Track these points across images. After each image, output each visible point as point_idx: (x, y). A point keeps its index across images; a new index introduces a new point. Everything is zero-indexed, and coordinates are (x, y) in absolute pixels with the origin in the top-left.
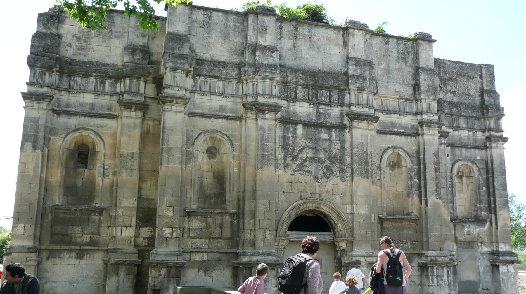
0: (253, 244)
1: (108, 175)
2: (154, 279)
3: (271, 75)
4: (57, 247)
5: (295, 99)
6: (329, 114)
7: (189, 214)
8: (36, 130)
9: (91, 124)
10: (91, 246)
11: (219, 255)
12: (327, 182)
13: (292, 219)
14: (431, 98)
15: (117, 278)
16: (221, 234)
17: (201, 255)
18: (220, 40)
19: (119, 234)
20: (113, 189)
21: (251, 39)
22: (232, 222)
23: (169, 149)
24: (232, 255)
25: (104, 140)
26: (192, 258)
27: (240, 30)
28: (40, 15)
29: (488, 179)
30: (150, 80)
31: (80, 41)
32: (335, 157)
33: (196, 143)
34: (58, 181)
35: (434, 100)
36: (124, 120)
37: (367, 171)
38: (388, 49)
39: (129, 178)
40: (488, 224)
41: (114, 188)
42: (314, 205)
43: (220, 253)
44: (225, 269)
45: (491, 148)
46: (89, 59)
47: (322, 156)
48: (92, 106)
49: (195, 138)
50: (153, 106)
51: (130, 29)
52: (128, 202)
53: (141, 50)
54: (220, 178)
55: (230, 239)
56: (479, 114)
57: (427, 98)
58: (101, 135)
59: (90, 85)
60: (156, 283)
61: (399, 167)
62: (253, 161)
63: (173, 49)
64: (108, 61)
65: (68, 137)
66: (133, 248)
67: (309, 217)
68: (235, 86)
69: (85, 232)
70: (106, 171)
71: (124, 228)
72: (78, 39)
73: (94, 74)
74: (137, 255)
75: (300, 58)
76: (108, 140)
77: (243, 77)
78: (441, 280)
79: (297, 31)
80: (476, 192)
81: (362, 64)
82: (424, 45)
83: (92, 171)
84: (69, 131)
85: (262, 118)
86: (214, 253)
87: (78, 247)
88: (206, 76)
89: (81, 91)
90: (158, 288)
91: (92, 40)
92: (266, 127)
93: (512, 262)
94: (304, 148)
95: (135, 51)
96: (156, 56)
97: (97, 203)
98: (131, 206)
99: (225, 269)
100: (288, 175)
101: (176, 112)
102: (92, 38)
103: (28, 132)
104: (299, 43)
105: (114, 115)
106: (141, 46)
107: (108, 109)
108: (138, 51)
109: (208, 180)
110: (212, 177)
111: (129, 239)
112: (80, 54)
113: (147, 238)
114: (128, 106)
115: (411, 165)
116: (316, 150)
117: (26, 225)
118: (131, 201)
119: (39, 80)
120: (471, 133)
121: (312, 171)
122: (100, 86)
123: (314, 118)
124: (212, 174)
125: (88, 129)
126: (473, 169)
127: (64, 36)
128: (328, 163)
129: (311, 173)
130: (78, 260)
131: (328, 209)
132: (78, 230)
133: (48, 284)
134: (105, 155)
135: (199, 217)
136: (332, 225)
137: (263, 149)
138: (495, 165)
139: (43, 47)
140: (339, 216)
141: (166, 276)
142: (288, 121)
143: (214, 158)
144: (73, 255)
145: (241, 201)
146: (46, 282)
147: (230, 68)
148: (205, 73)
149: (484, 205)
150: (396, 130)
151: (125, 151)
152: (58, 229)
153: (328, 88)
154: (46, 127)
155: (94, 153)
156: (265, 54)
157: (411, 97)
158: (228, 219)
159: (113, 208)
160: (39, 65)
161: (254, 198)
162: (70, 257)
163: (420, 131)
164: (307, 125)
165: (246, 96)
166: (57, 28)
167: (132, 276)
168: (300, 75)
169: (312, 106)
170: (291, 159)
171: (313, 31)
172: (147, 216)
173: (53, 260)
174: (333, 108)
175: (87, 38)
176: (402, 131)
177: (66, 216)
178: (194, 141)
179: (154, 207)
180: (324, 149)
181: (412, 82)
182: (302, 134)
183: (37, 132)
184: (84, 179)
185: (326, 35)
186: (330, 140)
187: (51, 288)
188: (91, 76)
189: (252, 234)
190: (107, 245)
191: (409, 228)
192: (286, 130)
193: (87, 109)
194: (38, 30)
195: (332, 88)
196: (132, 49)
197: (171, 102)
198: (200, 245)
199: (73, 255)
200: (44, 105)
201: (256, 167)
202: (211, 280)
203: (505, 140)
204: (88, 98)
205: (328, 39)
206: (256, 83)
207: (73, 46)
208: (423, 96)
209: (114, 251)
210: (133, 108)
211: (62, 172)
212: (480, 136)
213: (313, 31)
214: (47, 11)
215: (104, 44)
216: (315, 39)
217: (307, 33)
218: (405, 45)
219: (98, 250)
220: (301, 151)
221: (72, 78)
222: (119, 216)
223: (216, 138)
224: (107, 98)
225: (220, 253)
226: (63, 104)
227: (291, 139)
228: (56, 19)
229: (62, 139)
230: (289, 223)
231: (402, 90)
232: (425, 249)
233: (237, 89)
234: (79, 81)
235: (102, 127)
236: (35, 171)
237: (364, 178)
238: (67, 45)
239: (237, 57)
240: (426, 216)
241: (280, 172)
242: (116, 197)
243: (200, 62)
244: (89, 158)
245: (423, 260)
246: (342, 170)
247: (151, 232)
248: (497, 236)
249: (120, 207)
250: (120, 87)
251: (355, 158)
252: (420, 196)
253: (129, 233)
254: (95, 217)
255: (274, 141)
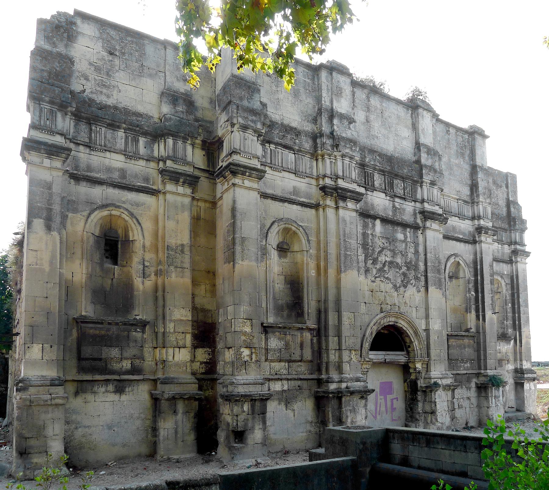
0: (339, 368)
1: (150, 275)
2: (235, 418)
3: (351, 153)
4: (89, 377)
5: (374, 189)
6: (404, 210)
7: (266, 329)
8: (49, 200)
9: (123, 199)
10: (133, 375)
11: (299, 383)
12: (405, 291)
13: (374, 336)
14: (488, 201)
15: (174, 418)
16: (302, 356)
17: (280, 383)
18: (290, 98)
19: (170, 358)
20: (159, 296)
21: (325, 102)
22: (312, 340)
23: (243, 240)
24: (313, 381)
25: (142, 225)
26: (271, 388)
27: (310, 89)
28: (41, 22)
29: (513, 295)
30: (199, 144)
31: (100, 74)
32: (411, 262)
33: (269, 234)
34: (84, 281)
35: (490, 204)
36: (168, 196)
37: (440, 280)
38: (449, 140)
39: (179, 280)
40: (512, 342)
41: (160, 293)
42: (393, 319)
43: (301, 379)
44: (307, 399)
45: (517, 262)
46: (115, 102)
47: (399, 260)
48: (123, 172)
49: (268, 227)
50: (204, 183)
51: (167, 67)
52: (180, 315)
53: (185, 100)
54: (295, 285)
55: (311, 361)
56: (507, 226)
57: (484, 201)
58: (137, 217)
59: (119, 141)
60: (239, 424)
61: (457, 278)
62: (335, 263)
63: (241, 99)
64: (140, 109)
65: (92, 216)
66: (190, 376)
67: (384, 333)
68: (309, 163)
69: (125, 355)
70: (146, 269)
71: (177, 350)
72: (98, 69)
73: (124, 126)
74: (197, 385)
75: (375, 137)
76: (148, 225)
77: (319, 152)
78: (498, 400)
79: (369, 101)
80: (504, 309)
81: (432, 153)
82: (478, 139)
83: (125, 269)
84: (94, 207)
85: (344, 208)
86: (295, 379)
87: (117, 377)
88: (277, 144)
89: (106, 149)
90: (242, 429)
91: (117, 74)
92: (348, 219)
93: (534, 379)
94: (383, 249)
95: (177, 100)
96: (201, 112)
97: (140, 313)
98: (185, 319)
99: (307, 399)
100: (369, 282)
101: (250, 189)
102: (117, 71)
103: (37, 203)
104: (372, 117)
105: (152, 189)
106: (182, 94)
107: (144, 179)
108: (181, 101)
109: (279, 285)
110: (283, 282)
111: (185, 364)
112: (101, 92)
113: (205, 363)
114: (175, 177)
115: (469, 275)
116: (394, 255)
117: (45, 345)
118: (183, 312)
119: (48, 123)
120: (500, 246)
121: (391, 277)
122: (132, 145)
123: (391, 213)
124: (282, 277)
125: (119, 207)
126: (501, 284)
127: (77, 60)
128: (404, 269)
129: (390, 279)
130: (118, 395)
131: (406, 325)
132: (115, 352)
133: (80, 430)
134: (144, 247)
135: (277, 333)
136: (405, 343)
137: (345, 247)
138: (520, 281)
139: (50, 73)
140: (416, 333)
141: (250, 412)
142: (367, 215)
143: (285, 257)
144: (111, 387)
145: (321, 314)
146: (76, 428)
147: (304, 138)
148: (277, 140)
149: (510, 322)
150: (456, 235)
151: (173, 241)
152: (88, 351)
153: (403, 178)
154: (63, 198)
155: (127, 242)
156: (343, 124)
157: (468, 199)
158: (307, 336)
159: (160, 322)
160: (47, 99)
161: (339, 311)
162: (107, 391)
163: (477, 239)
164: (385, 221)
165: (325, 176)
166: (66, 46)
167: (192, 415)
168: (378, 157)
169: (388, 198)
170: (371, 262)
171: (384, 104)
172: (205, 333)
173: (84, 396)
174: (407, 203)
175: (110, 70)
176: (461, 236)
177: (98, 332)
178: (267, 233)
179: (210, 321)
180: (401, 252)
181: (469, 182)
182: (381, 233)
183: (51, 204)
184: (114, 280)
185: (396, 112)
186: (405, 241)
187: (83, 436)
188: (119, 127)
189: (337, 355)
190: (155, 373)
191: (469, 346)
192: (365, 226)
193: (116, 176)
194: (38, 45)
195: (406, 178)
196: (173, 96)
197: (243, 174)
198: (279, 371)
199: (111, 387)
200: (57, 164)
201: (339, 271)
202: (292, 414)
203: (527, 254)
204: (117, 161)
205: (398, 117)
206: (334, 161)
207: (90, 78)
208: (481, 199)
209: (166, 381)
210: (181, 180)
211: (87, 268)
212: (507, 249)
213: (384, 104)
214: (49, 18)
215: (133, 83)
216: (386, 114)
217: (378, 106)
218: (463, 138)
219: (143, 380)
220: (380, 252)
221: (93, 128)
222: (170, 332)
223: (291, 229)
224: (142, 163)
225: (301, 379)
226: (83, 165)
227: (370, 237)
228: (65, 32)
229: (85, 218)
230: (371, 340)
231: (461, 189)
232: (482, 368)
233: (311, 168)
234: (103, 134)
235: (137, 205)
236: (51, 263)
237: (437, 288)
238: (82, 76)
239: (310, 125)
240: (484, 332)
241: (362, 278)
242: (164, 306)
243: (272, 125)
244: (119, 250)
245: (482, 379)
246: (417, 278)
247: (209, 354)
248: (521, 353)
249: (171, 321)
250: (161, 149)
251: (429, 264)
252: (477, 311)
253: (183, 355)
254: (137, 335)
255: (356, 238)
